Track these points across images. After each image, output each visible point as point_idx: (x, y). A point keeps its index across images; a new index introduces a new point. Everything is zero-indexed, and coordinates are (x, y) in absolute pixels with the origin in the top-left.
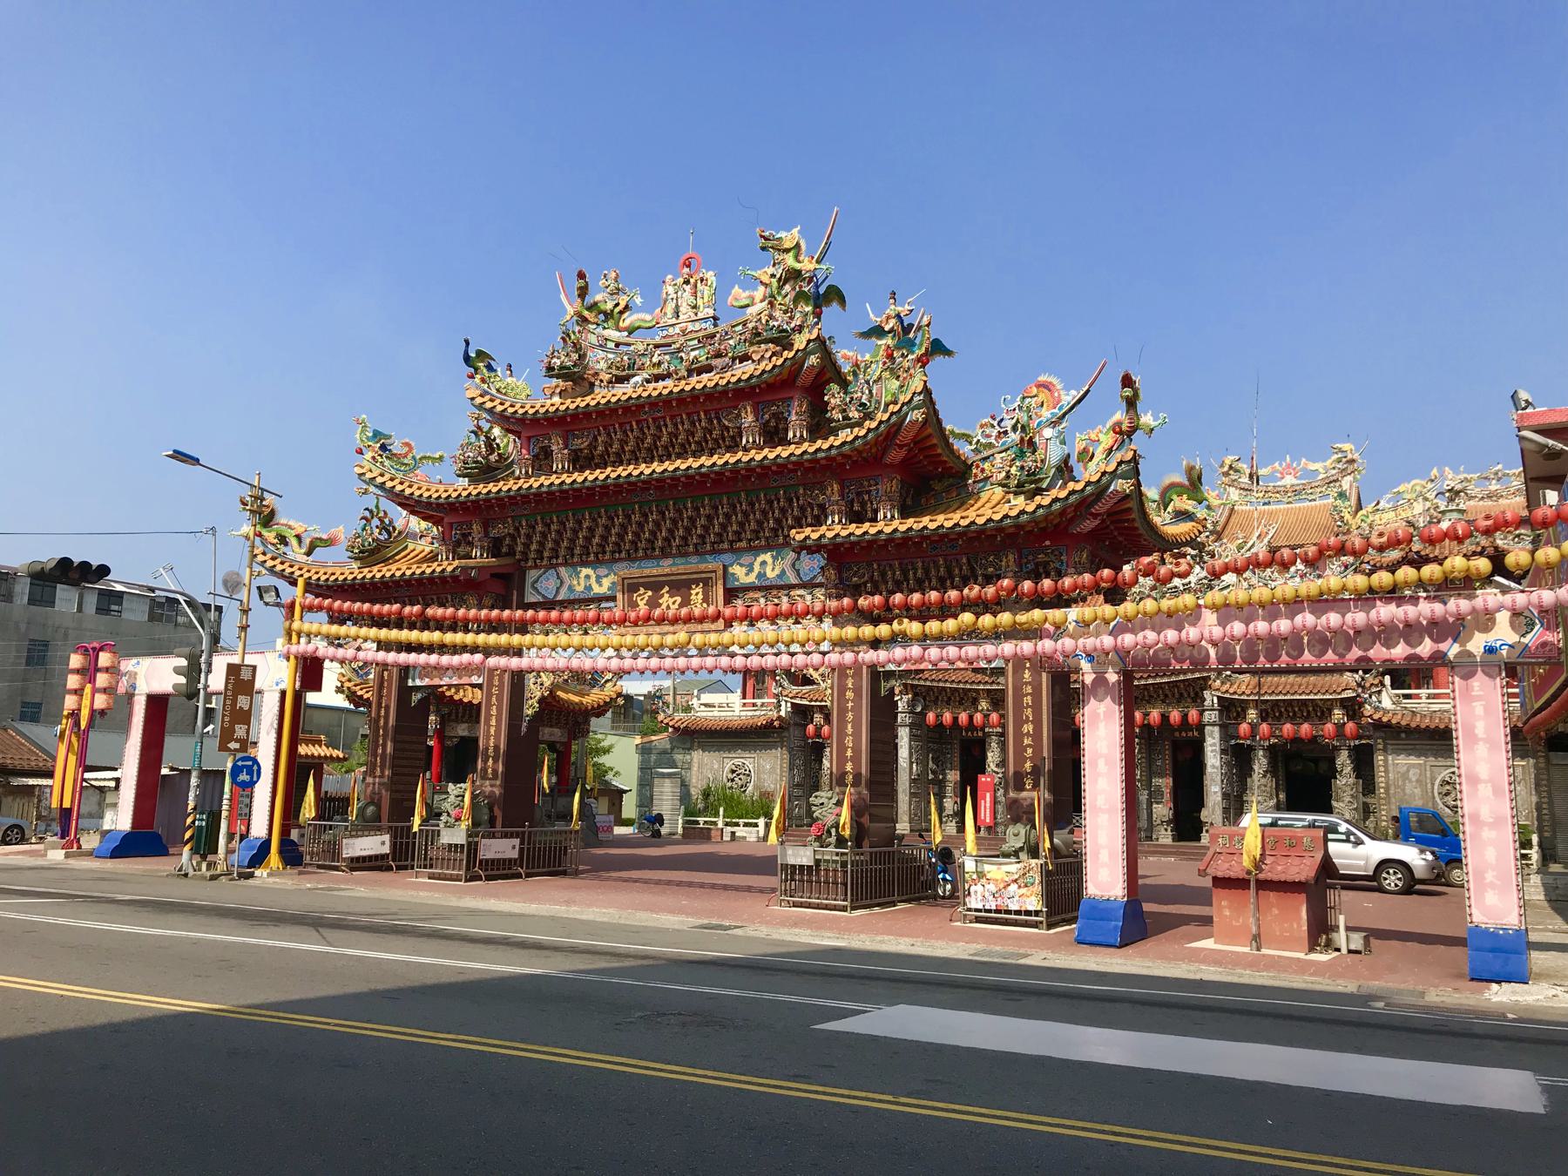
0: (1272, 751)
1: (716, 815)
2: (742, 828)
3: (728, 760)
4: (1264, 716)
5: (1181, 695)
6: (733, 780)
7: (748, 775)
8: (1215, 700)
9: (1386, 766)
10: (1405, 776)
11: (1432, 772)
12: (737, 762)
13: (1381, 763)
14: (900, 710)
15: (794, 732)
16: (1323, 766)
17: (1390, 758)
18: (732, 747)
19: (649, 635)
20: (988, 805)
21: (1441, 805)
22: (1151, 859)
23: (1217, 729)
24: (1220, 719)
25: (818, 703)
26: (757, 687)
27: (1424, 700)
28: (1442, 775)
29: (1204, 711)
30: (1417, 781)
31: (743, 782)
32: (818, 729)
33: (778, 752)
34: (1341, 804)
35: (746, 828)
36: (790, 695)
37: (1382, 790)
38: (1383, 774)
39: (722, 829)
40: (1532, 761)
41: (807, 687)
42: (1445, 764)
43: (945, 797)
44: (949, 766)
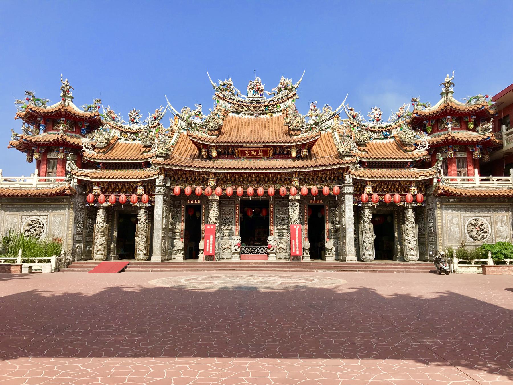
0: (108, 210)
1: (15, 254)
2: (36, 263)
3: (26, 217)
4: (375, 191)
5: (195, 179)
6: (29, 231)
7: (42, 227)
9: (442, 217)
10: (451, 222)
11: (464, 219)
12: (32, 218)
14: (157, 184)
15: (78, 199)
16: (133, 220)
17: (444, 212)
18: (32, 208)
21: (468, 237)
22: (320, 271)
23: (351, 196)
24: (354, 191)
25: (97, 180)
26: (48, 171)
27: (459, 182)
28: (469, 221)
29: (344, 186)
30: (457, 224)
31: (38, 232)
32: (96, 196)
33: (438, 212)
34: (409, 238)
35: (40, 264)
36: (77, 174)
37: (440, 230)
38: (440, 221)
39: (21, 266)
40: (511, 213)
41: (89, 170)
42: (470, 215)
43: (174, 239)
44: (178, 220)
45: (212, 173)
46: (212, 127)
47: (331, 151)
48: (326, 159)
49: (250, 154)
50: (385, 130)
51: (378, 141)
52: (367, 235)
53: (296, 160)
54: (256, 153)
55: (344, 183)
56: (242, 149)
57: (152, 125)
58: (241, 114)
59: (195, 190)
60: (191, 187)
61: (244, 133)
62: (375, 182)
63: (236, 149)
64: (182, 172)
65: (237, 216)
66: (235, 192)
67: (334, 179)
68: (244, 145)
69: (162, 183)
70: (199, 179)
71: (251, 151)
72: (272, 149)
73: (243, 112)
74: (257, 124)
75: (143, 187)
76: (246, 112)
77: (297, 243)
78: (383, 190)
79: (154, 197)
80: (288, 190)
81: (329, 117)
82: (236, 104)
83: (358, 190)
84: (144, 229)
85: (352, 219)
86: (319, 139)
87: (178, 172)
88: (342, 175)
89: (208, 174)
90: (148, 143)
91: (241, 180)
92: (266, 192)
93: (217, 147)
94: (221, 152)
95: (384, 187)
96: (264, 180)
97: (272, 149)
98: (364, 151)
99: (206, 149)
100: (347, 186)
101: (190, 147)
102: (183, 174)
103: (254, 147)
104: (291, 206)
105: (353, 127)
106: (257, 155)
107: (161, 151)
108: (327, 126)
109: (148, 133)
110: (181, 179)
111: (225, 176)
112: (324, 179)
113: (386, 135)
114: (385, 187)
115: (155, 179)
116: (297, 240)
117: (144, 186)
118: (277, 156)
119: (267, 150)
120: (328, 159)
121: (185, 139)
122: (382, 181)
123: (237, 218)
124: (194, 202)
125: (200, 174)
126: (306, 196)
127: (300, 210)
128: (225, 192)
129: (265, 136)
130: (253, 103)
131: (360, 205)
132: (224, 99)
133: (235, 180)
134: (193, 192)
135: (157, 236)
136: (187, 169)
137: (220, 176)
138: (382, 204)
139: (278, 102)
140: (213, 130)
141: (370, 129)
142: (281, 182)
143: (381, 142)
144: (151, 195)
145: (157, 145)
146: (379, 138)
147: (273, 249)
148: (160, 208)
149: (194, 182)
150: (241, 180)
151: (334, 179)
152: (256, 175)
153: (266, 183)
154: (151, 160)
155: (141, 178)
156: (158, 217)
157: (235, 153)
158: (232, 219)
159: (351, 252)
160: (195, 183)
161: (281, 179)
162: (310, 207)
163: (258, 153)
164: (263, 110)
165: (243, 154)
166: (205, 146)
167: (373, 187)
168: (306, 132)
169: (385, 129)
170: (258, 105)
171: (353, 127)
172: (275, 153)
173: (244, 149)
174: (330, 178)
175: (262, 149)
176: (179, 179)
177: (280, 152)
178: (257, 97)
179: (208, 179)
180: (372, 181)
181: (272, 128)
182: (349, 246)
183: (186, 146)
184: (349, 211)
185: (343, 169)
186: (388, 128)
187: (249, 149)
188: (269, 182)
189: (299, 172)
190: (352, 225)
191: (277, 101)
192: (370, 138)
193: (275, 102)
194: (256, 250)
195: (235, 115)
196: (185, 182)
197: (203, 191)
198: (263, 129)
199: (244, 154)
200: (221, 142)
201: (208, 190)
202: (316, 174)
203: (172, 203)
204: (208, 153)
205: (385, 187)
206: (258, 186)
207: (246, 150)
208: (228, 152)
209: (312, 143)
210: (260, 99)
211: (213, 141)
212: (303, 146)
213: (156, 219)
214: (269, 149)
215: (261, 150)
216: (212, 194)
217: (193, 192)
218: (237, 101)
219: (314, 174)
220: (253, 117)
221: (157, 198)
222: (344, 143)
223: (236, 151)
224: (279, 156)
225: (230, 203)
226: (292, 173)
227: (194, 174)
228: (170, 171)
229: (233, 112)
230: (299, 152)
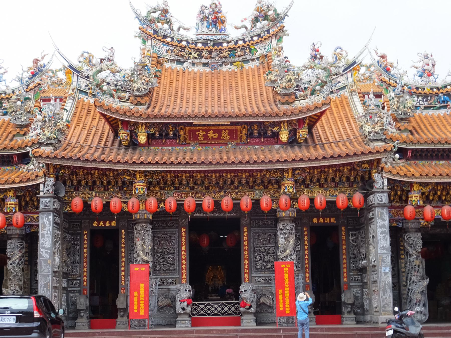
4: (427, 199)
5: (94, 182)
8: (386, 183)
13: (344, 257)
14: (42, 194)
19: (404, 123)
20: (142, 296)
23: (386, 211)
24: (390, 201)
45: (140, 172)
46: (138, 90)
47: (348, 130)
48: (340, 144)
49: (206, 137)
50: (442, 93)
51: (430, 112)
52: (414, 278)
53: (289, 148)
54: (217, 134)
55: (372, 187)
56: (192, 128)
57: (28, 86)
58: (185, 65)
59: (109, 202)
60: (102, 198)
61: (194, 99)
62: (426, 185)
63: (181, 129)
64: (86, 171)
65: (184, 248)
66: (180, 206)
67: (355, 180)
68: (196, 122)
69: (51, 191)
70: (116, 183)
71: (207, 131)
72: (245, 128)
73: (190, 61)
74: (216, 81)
75: (16, 198)
76: (196, 61)
77: (287, 295)
78: (440, 197)
79: (36, 216)
80: (275, 200)
81: (343, 69)
82: (177, 46)
83: (397, 198)
84: (20, 275)
85: (387, 250)
86: (328, 111)
87: (77, 171)
88: (370, 173)
89: (133, 174)
90: (22, 120)
91: (191, 184)
92: (236, 206)
93: (148, 126)
94: (153, 135)
95: (442, 194)
96: (232, 183)
97: (245, 128)
98: (406, 130)
99: (127, 129)
100: (378, 192)
101: (95, 125)
102: (87, 174)
103: (213, 125)
104: (281, 230)
105: (387, 88)
106: (219, 138)
107: (48, 134)
108: (340, 84)
109: (22, 103)
110: (83, 183)
111: (163, 177)
112: (337, 179)
113: (444, 102)
114: (444, 194)
115: (38, 185)
116: (287, 289)
117: (18, 197)
118: (253, 140)
119: (236, 130)
120: (344, 144)
121: (86, 111)
122: (437, 184)
123: (183, 252)
124: (104, 223)
125: (118, 175)
126: (306, 211)
127: (296, 236)
128: (162, 205)
129: (232, 105)
130: (207, 43)
131: (400, 225)
132: (154, 37)
133: (180, 183)
134: (107, 205)
135: (44, 287)
136: (94, 165)
137: (153, 177)
138: (438, 223)
139: (252, 42)
140: (139, 96)
141: (415, 90)
142: (262, 187)
143: (436, 112)
144: (30, 213)
145: (40, 124)
146: (431, 107)
147: (250, 307)
148: (48, 237)
149: (106, 189)
150: (191, 184)
151: (355, 180)
152: (218, 175)
153: (235, 189)
154: (30, 150)
155: (13, 182)
156: (46, 252)
157: (179, 136)
158: (174, 253)
159: (388, 309)
160: (108, 189)
161: (262, 182)
162: (314, 230)
163: (220, 135)
164: (225, 57)
165: (194, 136)
166: (126, 124)
167: (423, 194)
168: (305, 97)
169: (441, 91)
170: (216, 47)
171: (387, 88)
172: (250, 135)
173: (195, 128)
174: (348, 179)
175: (228, 127)
176: (79, 182)
177: (259, 133)
178: (214, 33)
179: (131, 183)
180: (421, 184)
181: (243, 89)
182: (384, 297)
183: (89, 124)
184: (382, 236)
185: (370, 162)
186: (446, 89)
187: (204, 128)
188: (241, 188)
189: (294, 170)
190: (388, 260)
191: (250, 42)
192: (416, 107)
193: (248, 43)
194: (226, 309)
195: (175, 65)
196: (92, 189)
197: (124, 205)
198: (228, 92)
199: (196, 138)
200: (155, 117)
201: (133, 202)
202: (325, 172)
203: (67, 225)
204: (131, 137)
205: (444, 194)
206: (222, 193)
207: (199, 131)
208: (167, 134)
209: (317, 118)
210: (220, 37)
211: (141, 115)
212: (301, 122)
213: (42, 257)
214: (239, 127)
215: (225, 130)
216: (139, 210)
217: (107, 205)
218: (178, 41)
219: (321, 172)
220: (208, 69)
221: (42, 218)
222: (371, 118)
223: (182, 133)
224: (258, 140)
225: (170, 224)
226: (282, 171)
227: (106, 174)
228: (64, 169)
229: (173, 61)
230: (293, 133)
